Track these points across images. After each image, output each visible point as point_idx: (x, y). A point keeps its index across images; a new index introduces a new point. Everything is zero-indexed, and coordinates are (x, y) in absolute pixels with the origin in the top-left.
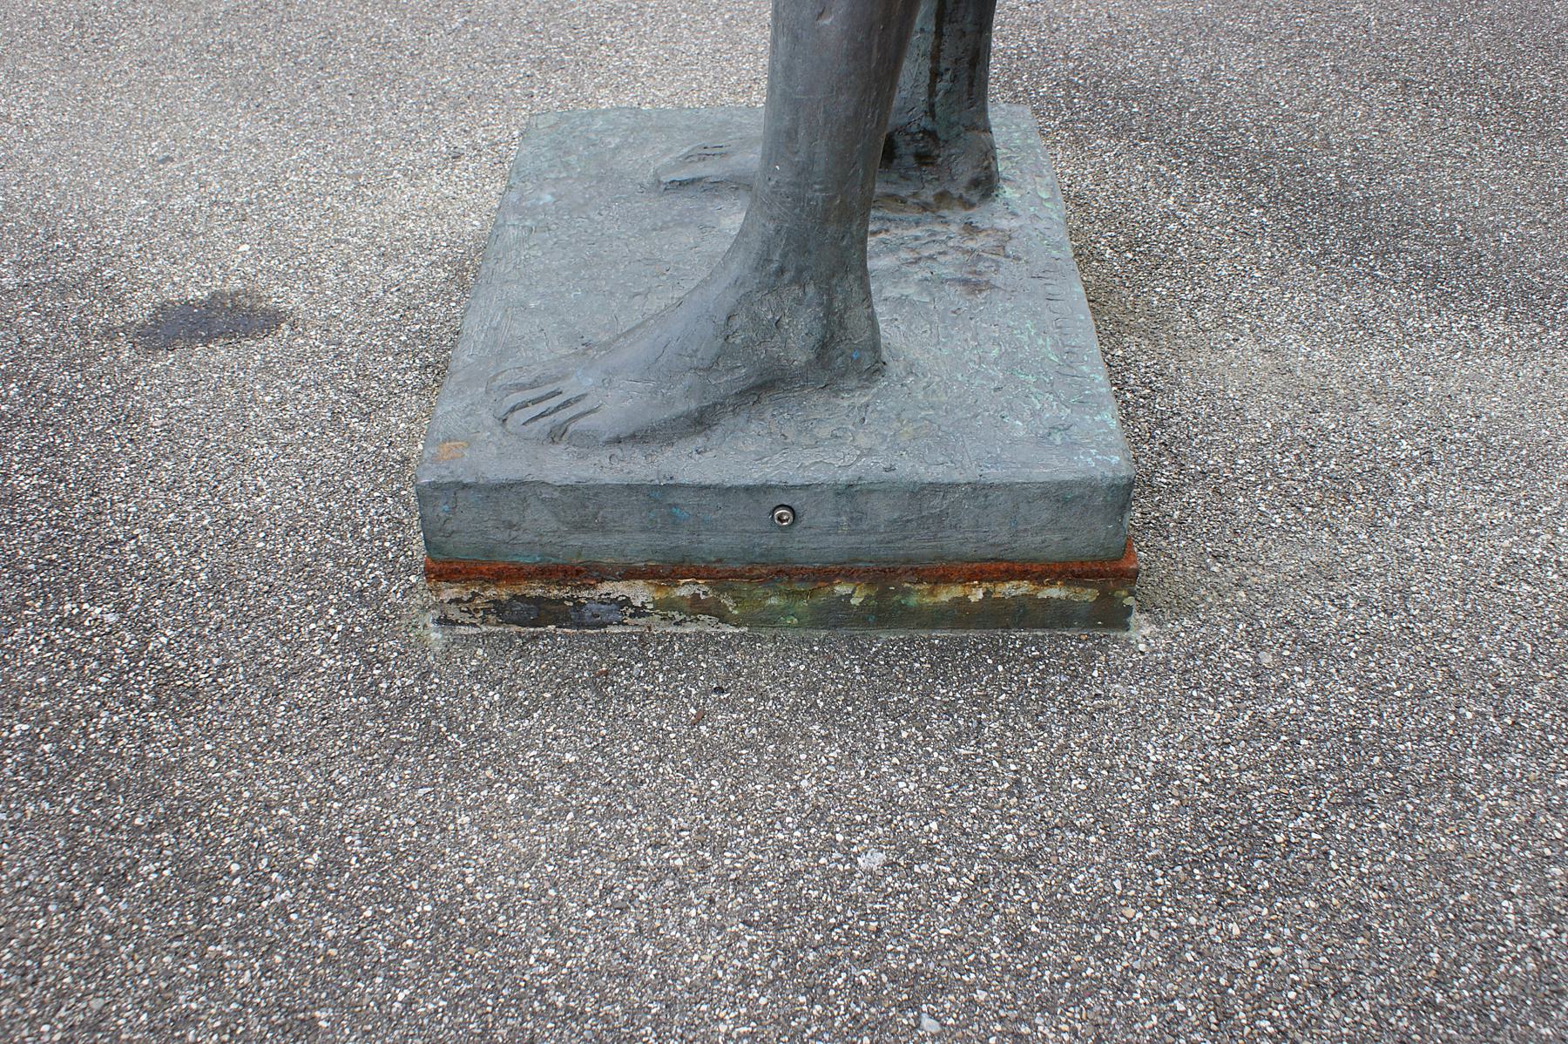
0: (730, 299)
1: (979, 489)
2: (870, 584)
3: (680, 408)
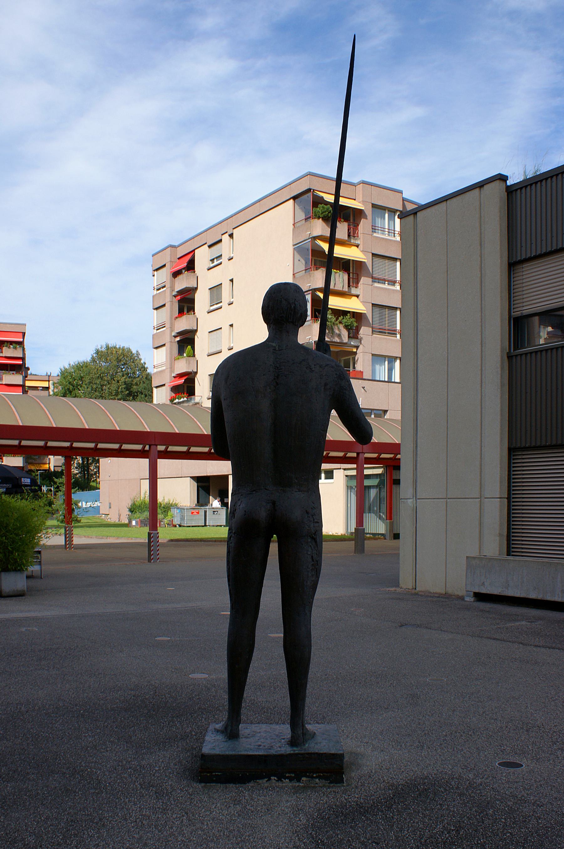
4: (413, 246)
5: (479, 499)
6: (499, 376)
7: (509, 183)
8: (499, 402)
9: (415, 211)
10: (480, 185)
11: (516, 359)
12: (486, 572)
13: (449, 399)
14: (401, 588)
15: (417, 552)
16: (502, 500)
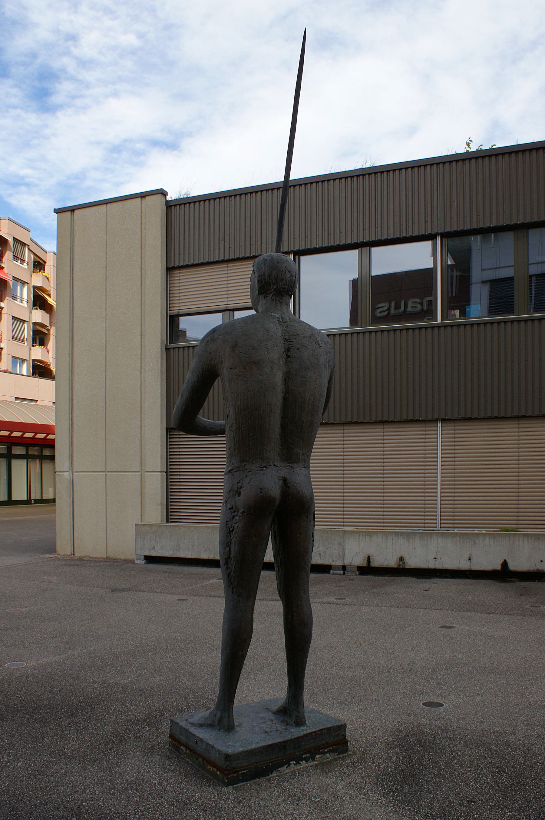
4: (70, 239)
5: (140, 473)
6: (159, 365)
7: (169, 198)
8: (160, 387)
9: (73, 209)
10: (143, 196)
11: (173, 351)
12: (156, 538)
13: (107, 382)
14: (59, 554)
15: (74, 521)
16: (162, 473)
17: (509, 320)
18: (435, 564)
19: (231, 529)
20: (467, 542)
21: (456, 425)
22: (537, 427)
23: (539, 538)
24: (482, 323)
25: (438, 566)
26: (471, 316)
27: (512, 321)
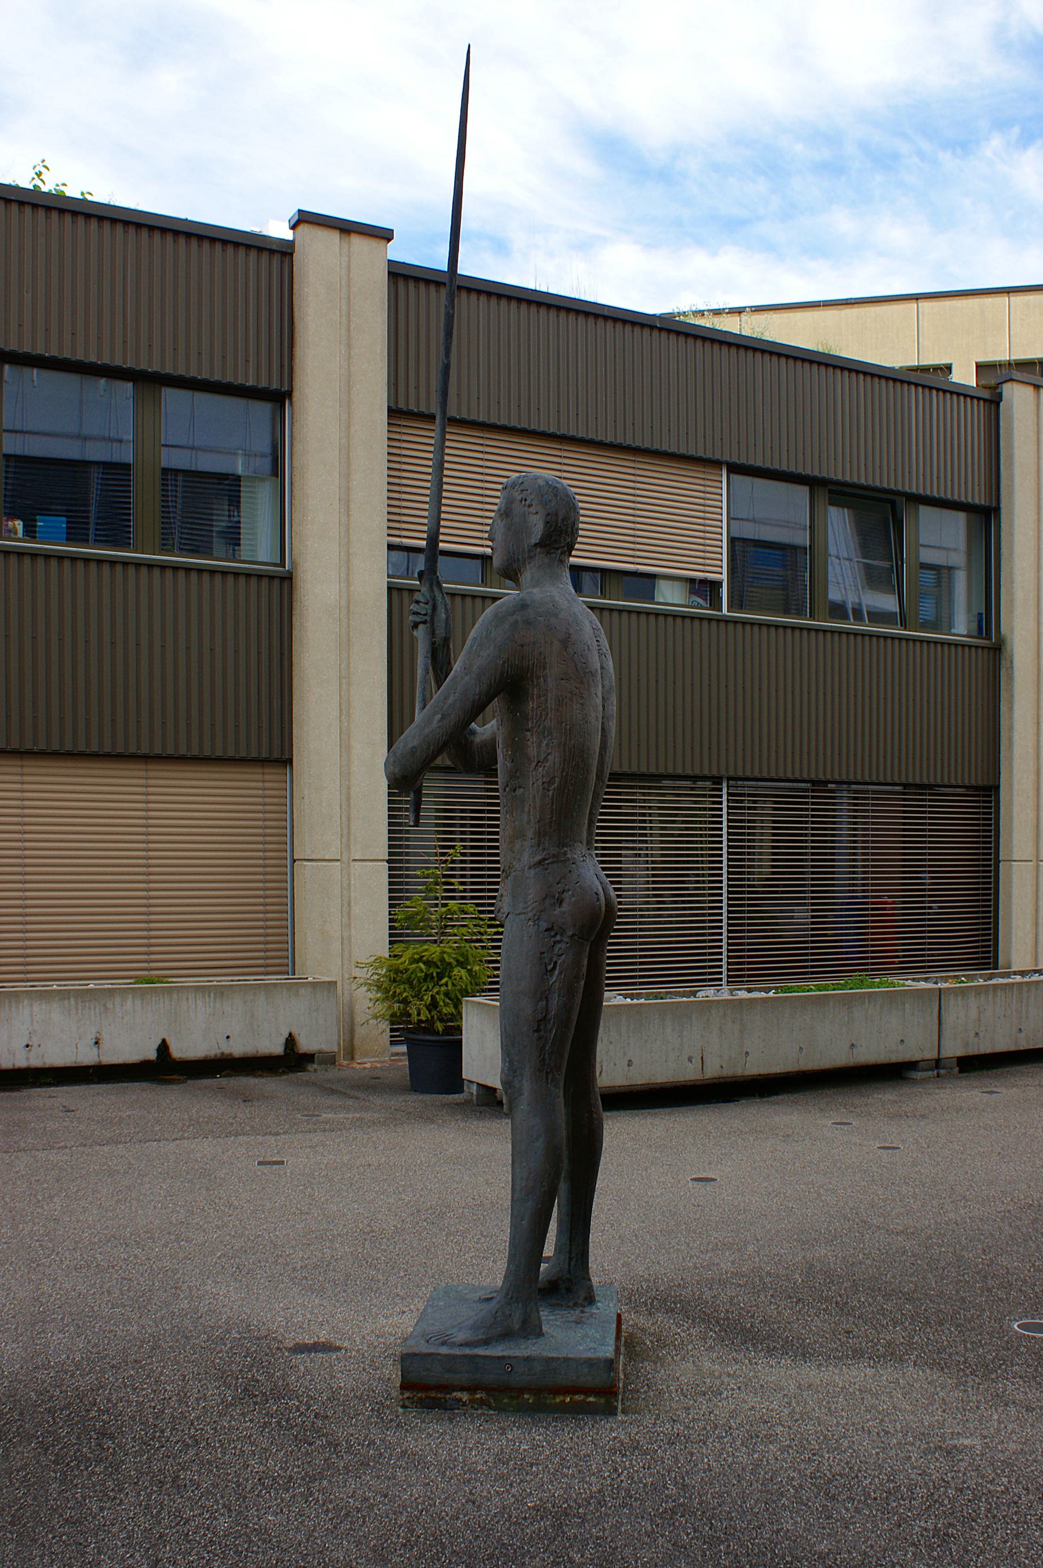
0: (497, 1306)
1: (566, 1360)
2: (535, 1394)
3: (480, 1337)
17: (27, 551)
18: (27, 1059)
19: (550, 967)
20: (90, 1008)
21: (266, 771)
22: (178, 779)
23: (222, 994)
24: (28, 554)
25: (36, 1062)
26: (953, 631)
27: (126, 563)
